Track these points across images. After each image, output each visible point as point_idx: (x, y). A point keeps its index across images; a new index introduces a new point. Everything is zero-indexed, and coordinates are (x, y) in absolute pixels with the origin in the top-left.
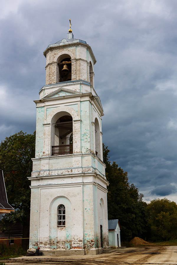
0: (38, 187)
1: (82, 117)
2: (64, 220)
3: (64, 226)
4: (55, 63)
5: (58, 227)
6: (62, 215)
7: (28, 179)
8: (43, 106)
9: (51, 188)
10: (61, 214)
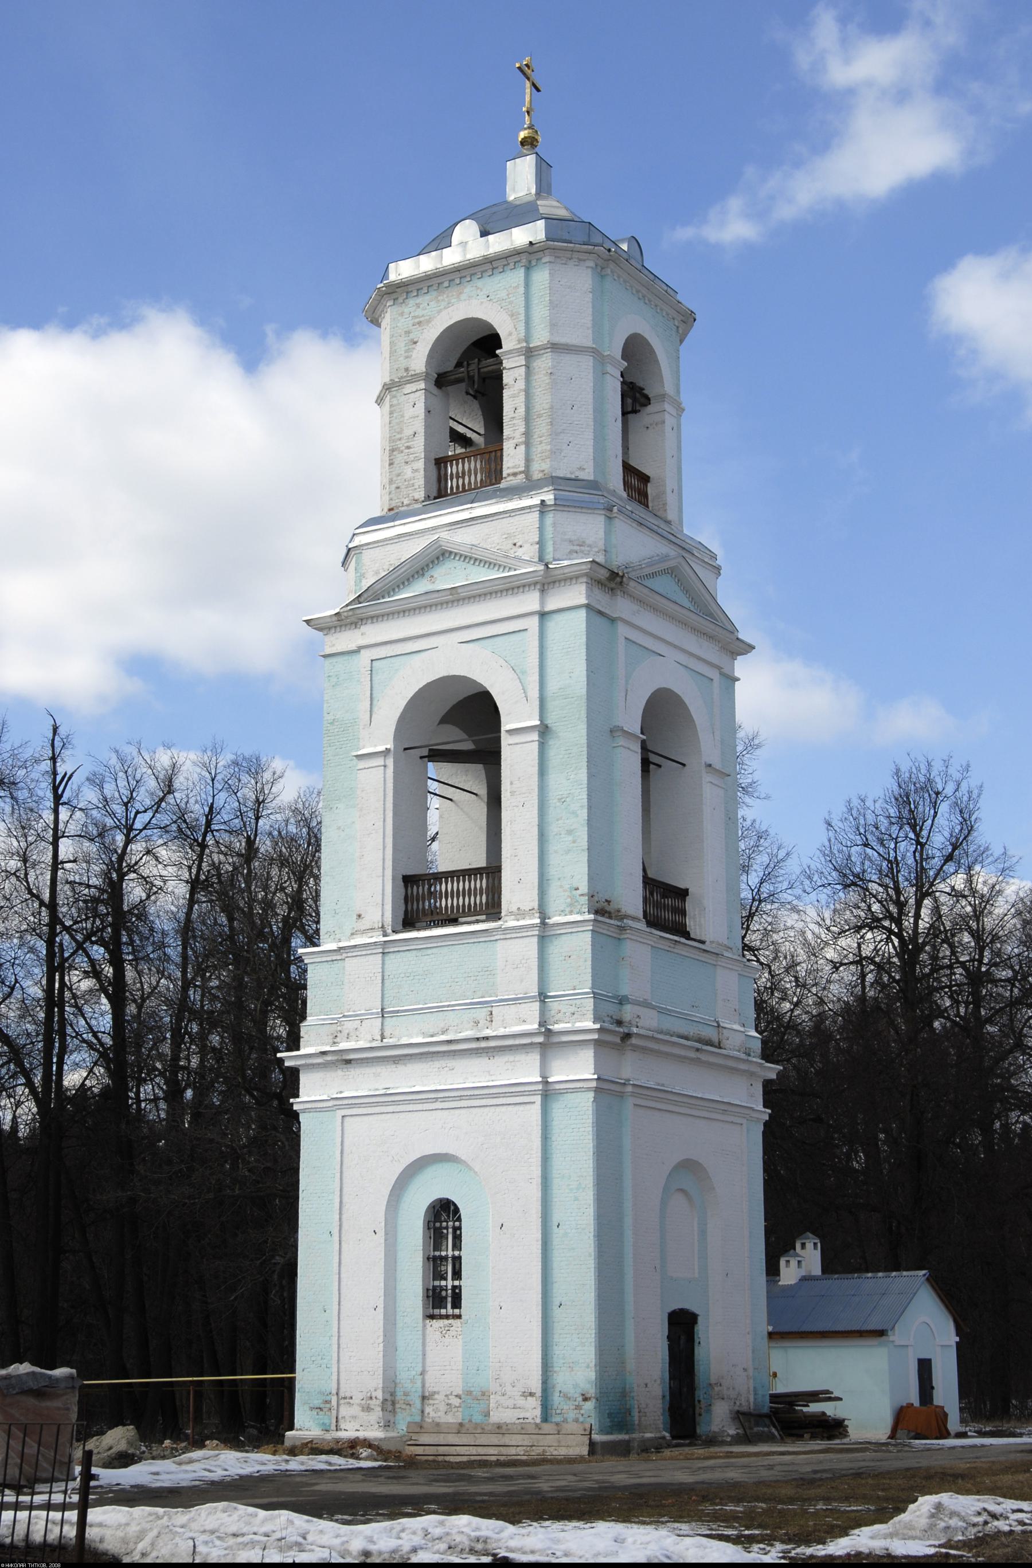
0: (339, 1103)
1: (551, 705)
2: (456, 1283)
3: (457, 1311)
4: (414, 379)
5: (432, 1317)
6: (450, 1253)
7: (292, 1104)
8: (352, 646)
9: (390, 1109)
10: (446, 1279)
